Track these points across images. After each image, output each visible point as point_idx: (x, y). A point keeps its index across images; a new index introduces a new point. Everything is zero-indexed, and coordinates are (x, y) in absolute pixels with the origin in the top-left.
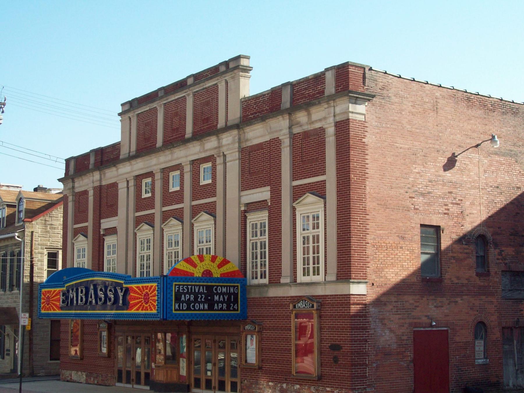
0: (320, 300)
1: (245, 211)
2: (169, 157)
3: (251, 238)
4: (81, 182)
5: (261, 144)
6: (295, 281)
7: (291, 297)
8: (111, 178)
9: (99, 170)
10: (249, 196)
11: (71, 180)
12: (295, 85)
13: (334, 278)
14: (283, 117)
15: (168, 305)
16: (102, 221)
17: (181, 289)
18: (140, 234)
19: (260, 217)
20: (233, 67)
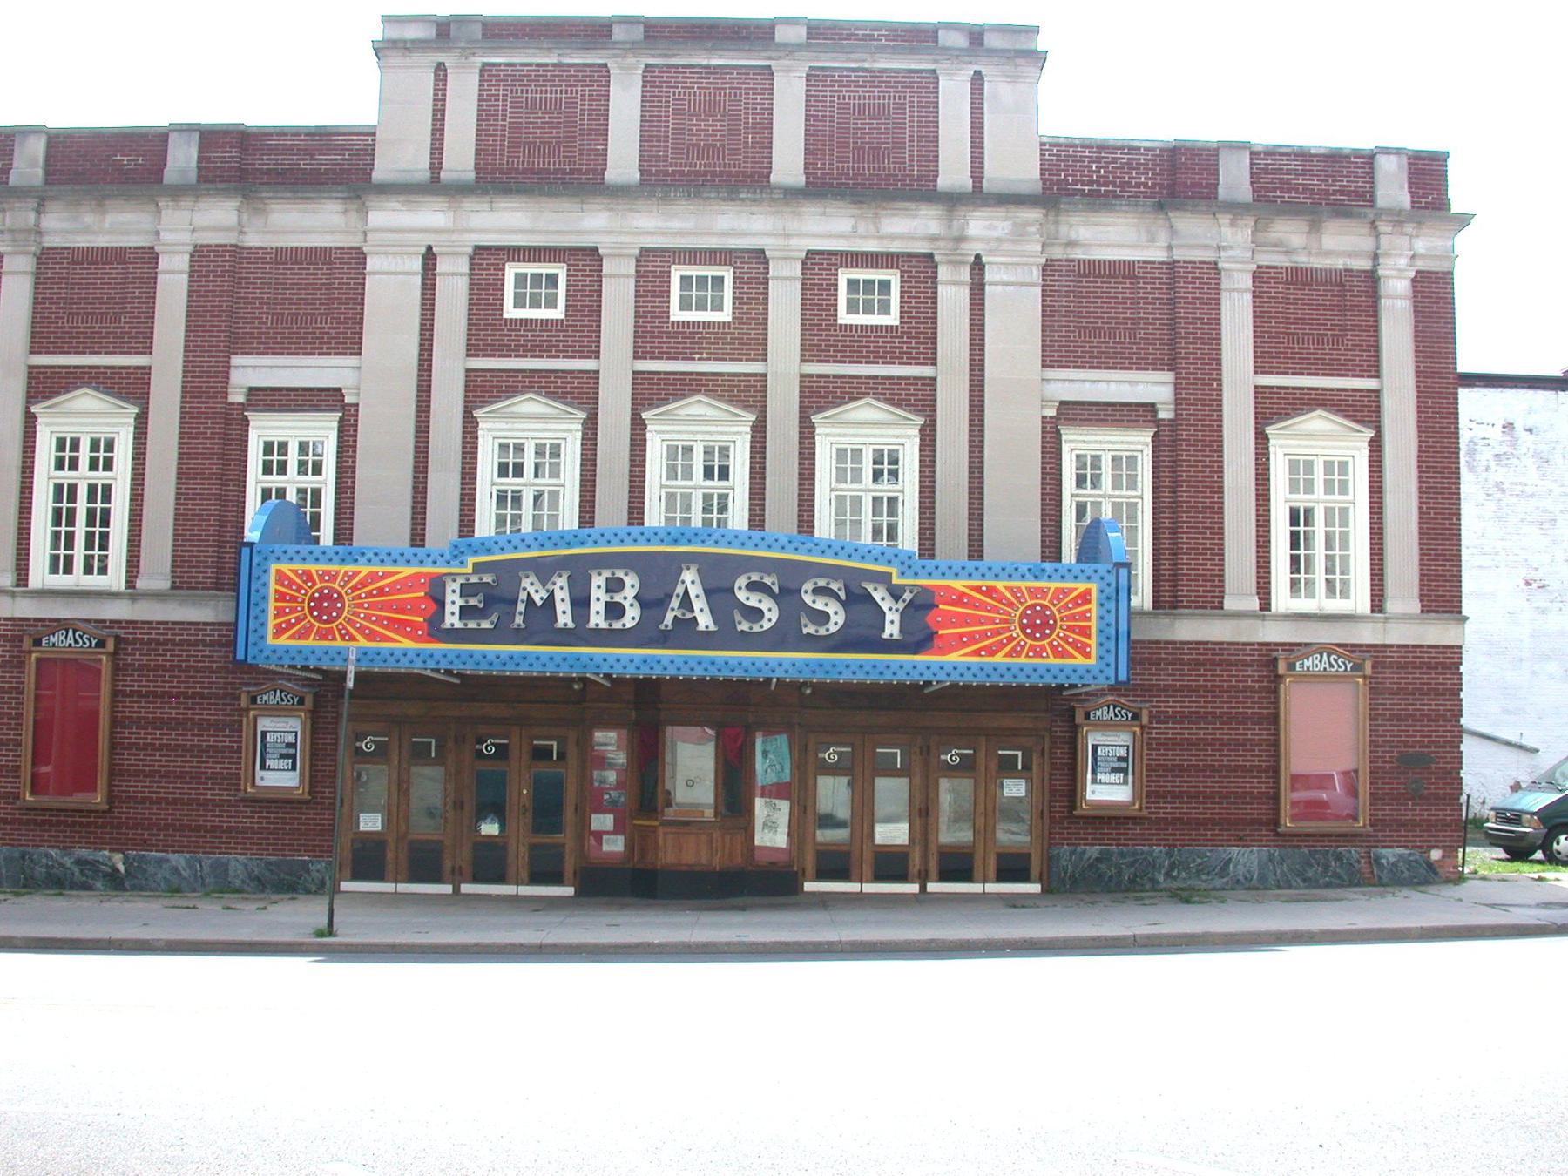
0: (121, 632)
1: (1057, 418)
2: (688, 223)
3: (664, 482)
4: (89, 219)
5: (324, 250)
6: (1265, 604)
7: (1260, 644)
8: (1191, 247)
9: (244, 197)
10: (1077, 385)
11: (33, 203)
12: (1259, 153)
13: (164, 583)
14: (1046, 216)
15: (252, 638)
16: (236, 360)
17: (599, 597)
18: (828, 430)
19: (845, 435)
20: (1017, 50)
